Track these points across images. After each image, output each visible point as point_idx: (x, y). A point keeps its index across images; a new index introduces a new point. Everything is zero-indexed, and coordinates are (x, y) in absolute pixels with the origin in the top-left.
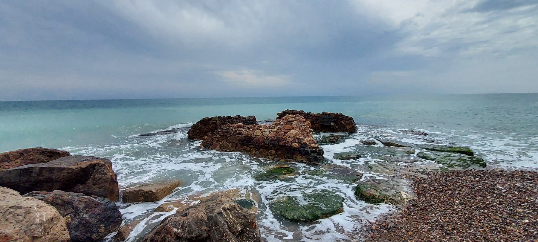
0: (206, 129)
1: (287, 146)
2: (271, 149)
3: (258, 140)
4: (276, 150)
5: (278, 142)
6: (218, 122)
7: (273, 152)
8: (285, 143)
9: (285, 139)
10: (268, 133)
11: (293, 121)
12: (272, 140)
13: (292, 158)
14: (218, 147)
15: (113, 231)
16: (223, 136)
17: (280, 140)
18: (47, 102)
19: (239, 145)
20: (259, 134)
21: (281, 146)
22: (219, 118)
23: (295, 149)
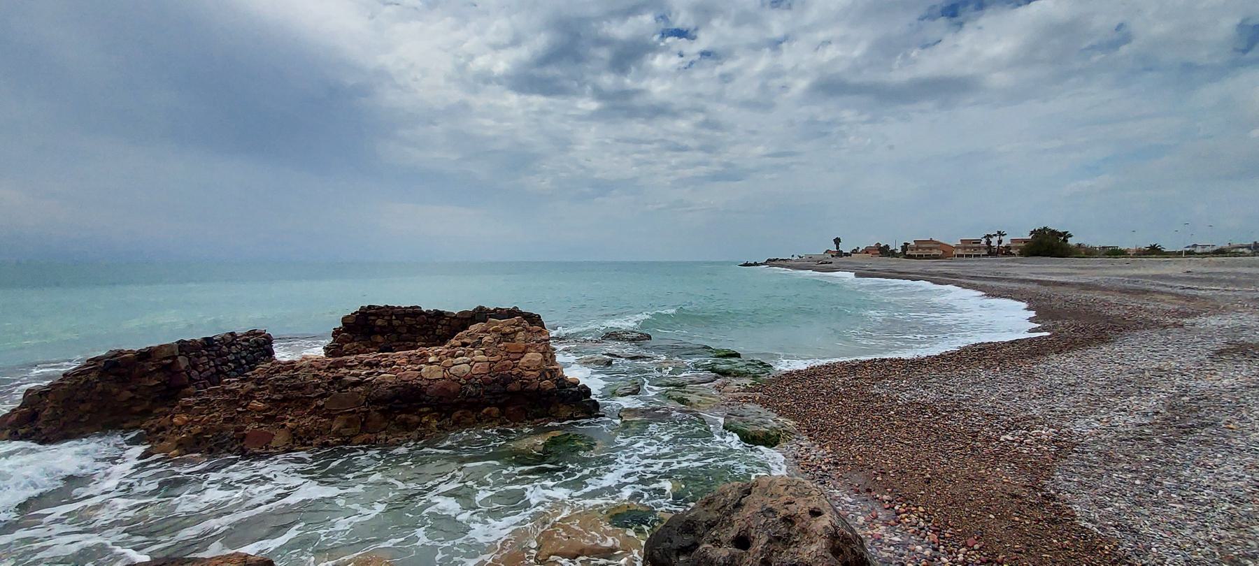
0: (128, 394)
1: (530, 391)
2: (490, 405)
3: (443, 389)
4: (502, 407)
5: (504, 385)
6: (183, 362)
7: (495, 410)
8: (522, 383)
9: (520, 375)
10: (466, 367)
11: (515, 332)
12: (486, 383)
13: (548, 415)
14: (280, 438)
15: (798, 358)
16: (284, 400)
17: (508, 380)
18: (634, 265)
19: (375, 416)
20: (439, 375)
21: (512, 393)
22: (182, 345)
23: (550, 393)
